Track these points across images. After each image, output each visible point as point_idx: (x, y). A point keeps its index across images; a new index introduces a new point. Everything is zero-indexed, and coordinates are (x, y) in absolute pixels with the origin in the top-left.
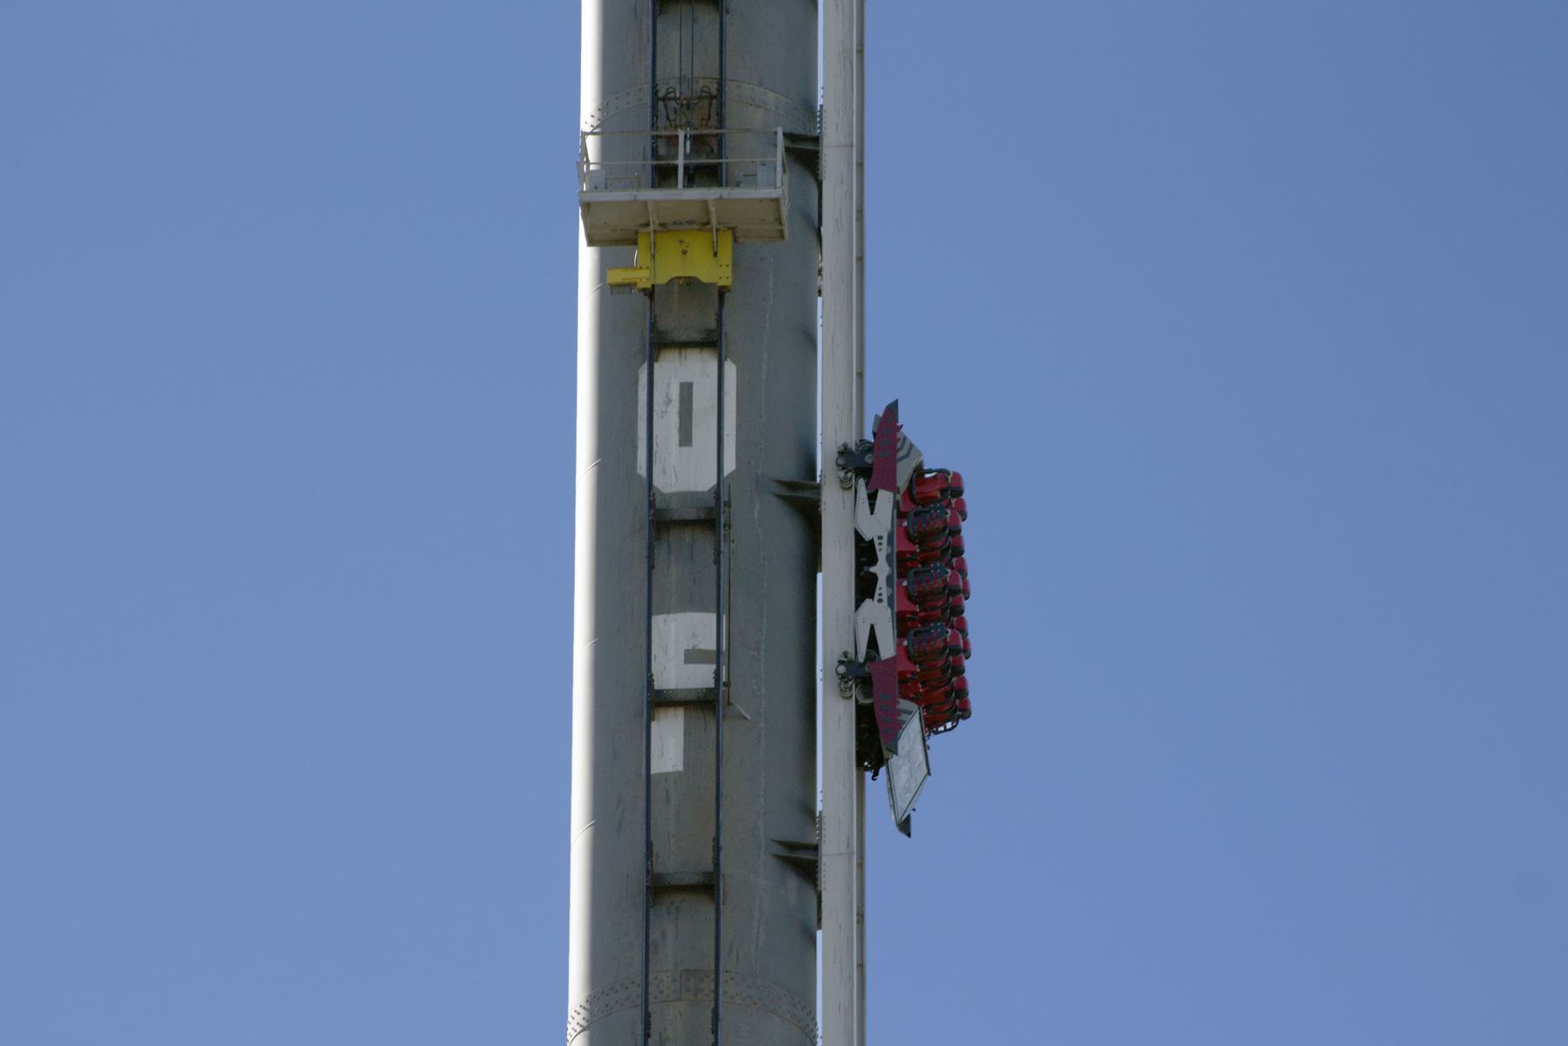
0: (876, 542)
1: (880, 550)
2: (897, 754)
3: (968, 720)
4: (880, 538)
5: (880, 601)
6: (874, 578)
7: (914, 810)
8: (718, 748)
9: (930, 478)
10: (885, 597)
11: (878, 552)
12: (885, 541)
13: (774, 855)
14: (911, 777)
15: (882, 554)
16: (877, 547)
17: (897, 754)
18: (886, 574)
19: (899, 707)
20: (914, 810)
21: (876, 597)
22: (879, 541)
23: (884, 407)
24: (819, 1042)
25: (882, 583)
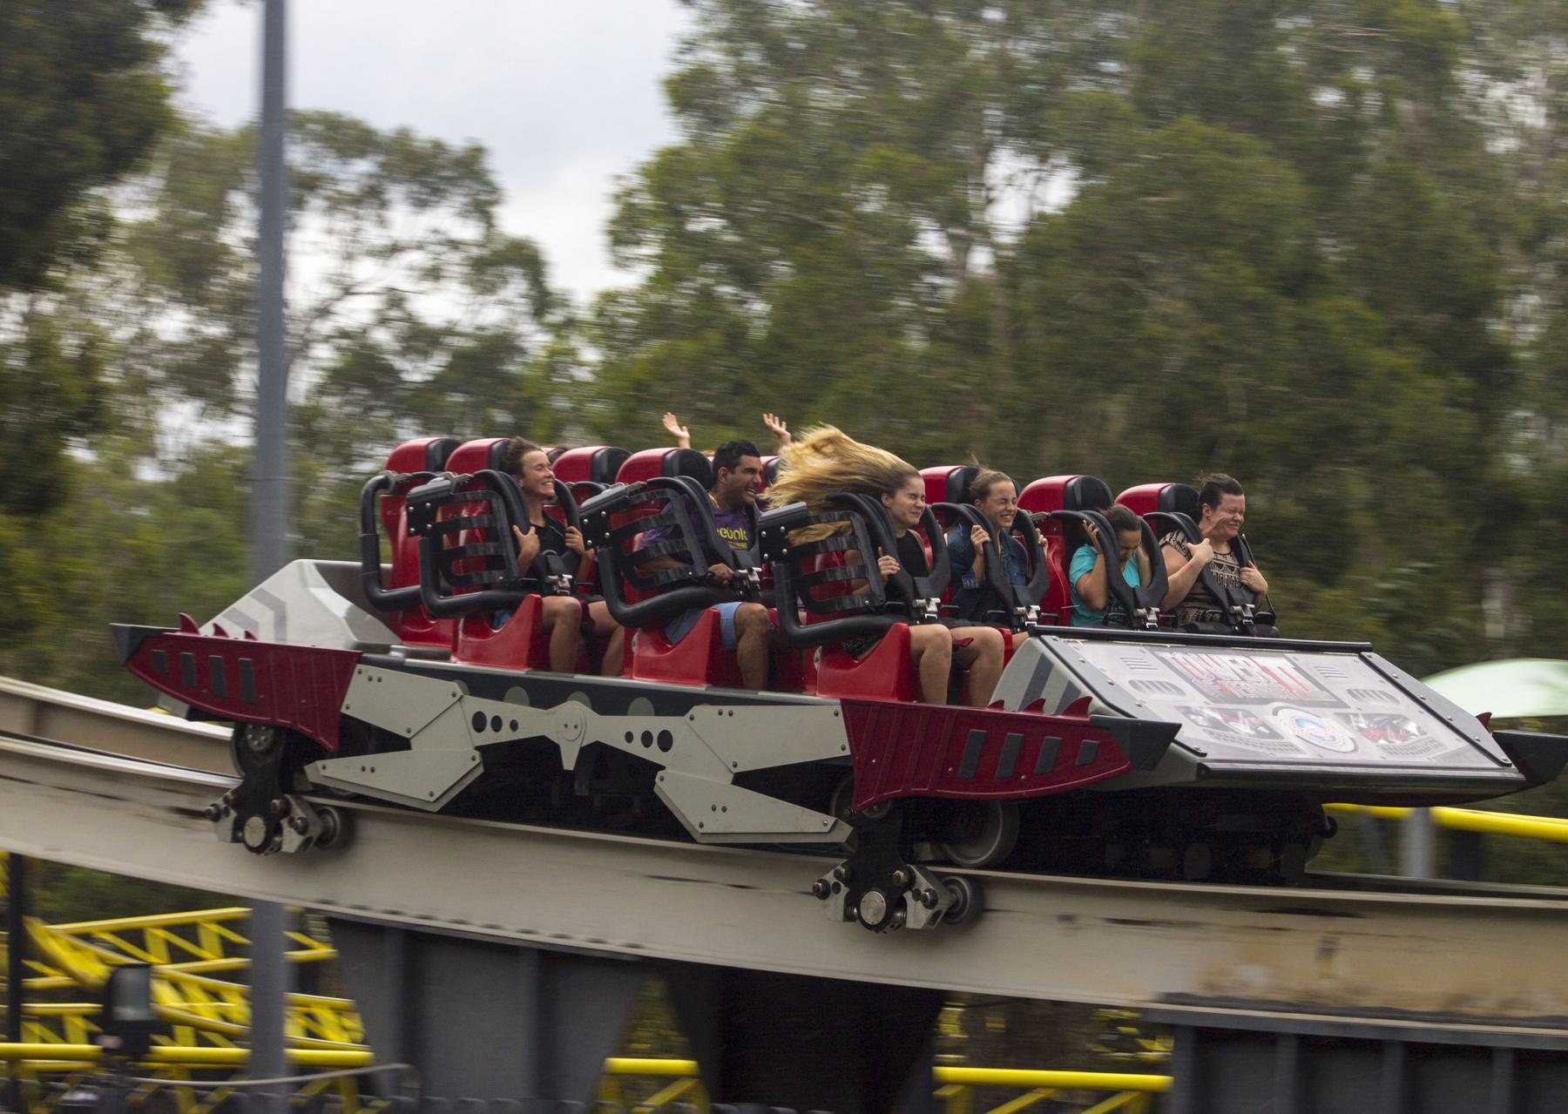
0: (489, 737)
1: (514, 725)
2: (1176, 728)
3: (482, 711)
4: (479, 722)
5: (666, 741)
6: (596, 754)
7: (731, 714)
8: (429, 724)
9: (814, 560)
10: (656, 724)
11: (520, 735)
12: (490, 708)
13: (526, 353)
14: (1340, 704)
15: (530, 722)
16: (506, 735)
17: (1176, 728)
18: (588, 712)
19: (1013, 707)
20: (731, 714)
21: (653, 754)
22: (489, 727)
23: (595, 740)
24: (1566, 1049)
25: (613, 730)
